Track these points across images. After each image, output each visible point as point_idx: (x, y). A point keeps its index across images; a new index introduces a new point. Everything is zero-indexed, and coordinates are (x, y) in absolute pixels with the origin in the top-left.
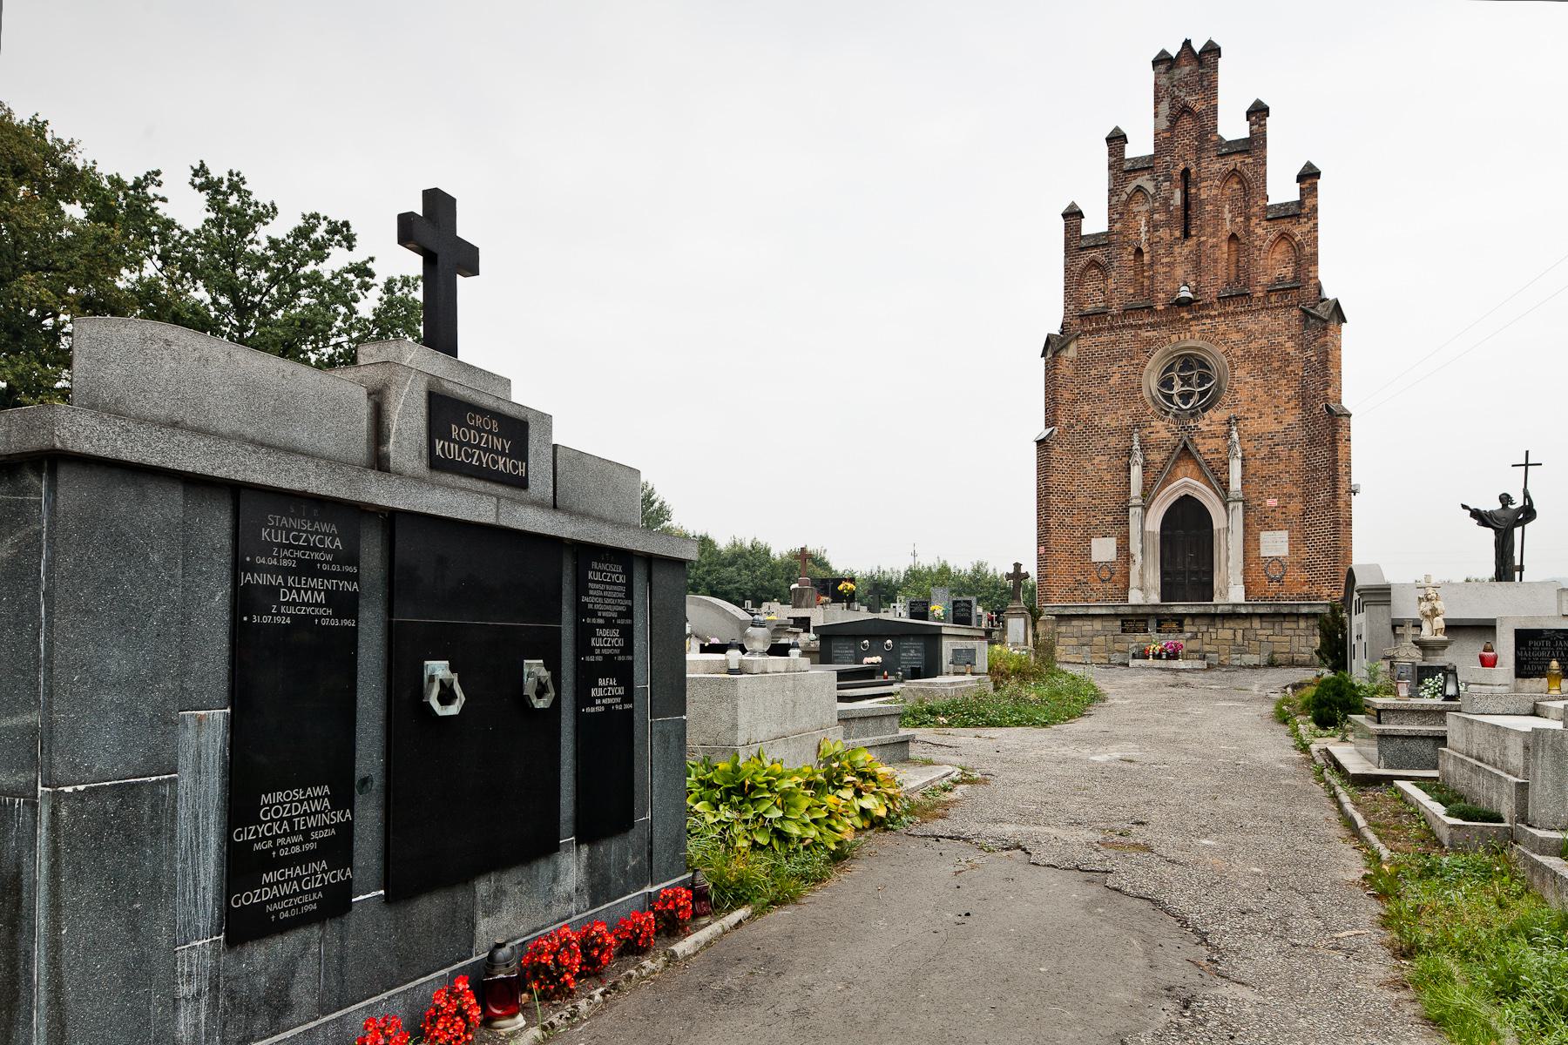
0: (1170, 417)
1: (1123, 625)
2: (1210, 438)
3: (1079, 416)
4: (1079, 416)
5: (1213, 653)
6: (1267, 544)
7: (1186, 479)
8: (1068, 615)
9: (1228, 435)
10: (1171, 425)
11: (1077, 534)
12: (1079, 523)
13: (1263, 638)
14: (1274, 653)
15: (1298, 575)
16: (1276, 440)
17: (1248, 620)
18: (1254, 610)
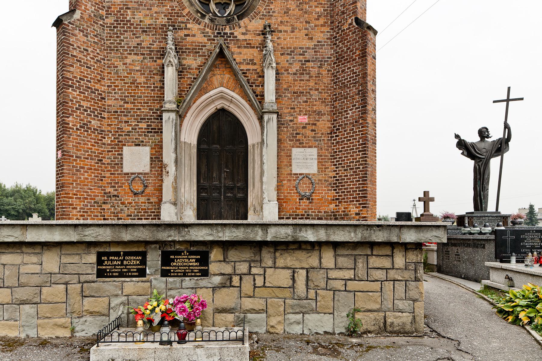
0: (207, 20)
1: (100, 262)
2: (245, 47)
3: (109, 8)
4: (109, 8)
5: (258, 312)
6: (298, 161)
7: (222, 89)
9: (263, 45)
10: (207, 30)
11: (107, 141)
12: (109, 129)
13: (339, 285)
14: (356, 310)
15: (325, 193)
16: (308, 56)
17: (316, 253)
18: (328, 235)
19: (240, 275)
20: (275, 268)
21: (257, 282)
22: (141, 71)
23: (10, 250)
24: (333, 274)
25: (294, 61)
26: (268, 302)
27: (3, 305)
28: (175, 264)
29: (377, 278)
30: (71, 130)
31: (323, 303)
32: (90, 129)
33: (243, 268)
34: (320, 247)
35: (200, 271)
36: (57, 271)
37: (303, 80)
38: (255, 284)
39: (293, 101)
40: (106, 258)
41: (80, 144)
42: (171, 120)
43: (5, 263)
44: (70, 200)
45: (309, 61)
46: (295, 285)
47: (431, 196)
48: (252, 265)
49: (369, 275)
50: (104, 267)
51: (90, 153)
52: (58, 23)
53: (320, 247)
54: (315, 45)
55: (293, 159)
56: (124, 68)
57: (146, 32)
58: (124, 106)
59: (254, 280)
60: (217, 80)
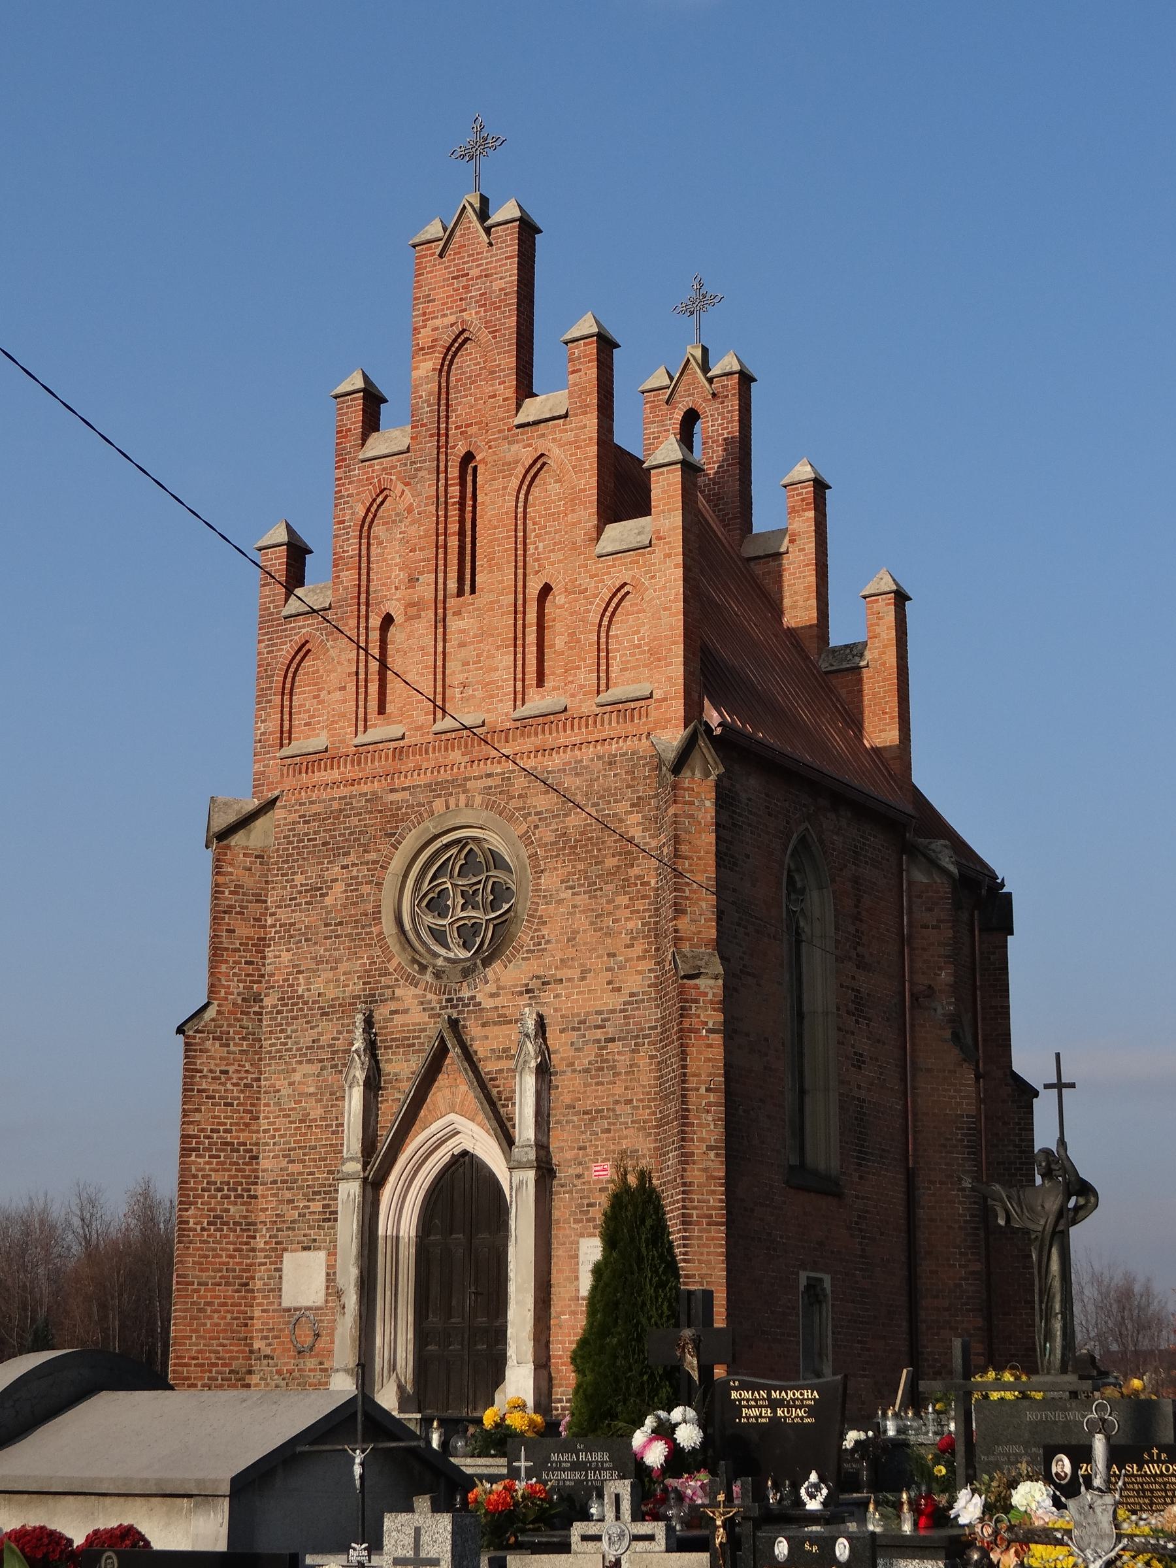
2: (495, 1023)
7: (452, 1117)
16: (610, 1031)
22: (317, 1094)
25: (585, 1043)
30: (191, 1234)
32: (227, 1224)
37: (602, 1084)
39: (582, 1132)
41: (207, 1257)
42: (352, 1197)
44: (185, 1369)
45: (613, 1040)
51: (225, 1273)
52: (180, 1030)
54: (625, 1003)
55: (580, 1262)
56: (290, 1091)
57: (327, 1014)
58: (286, 1169)
60: (444, 1099)
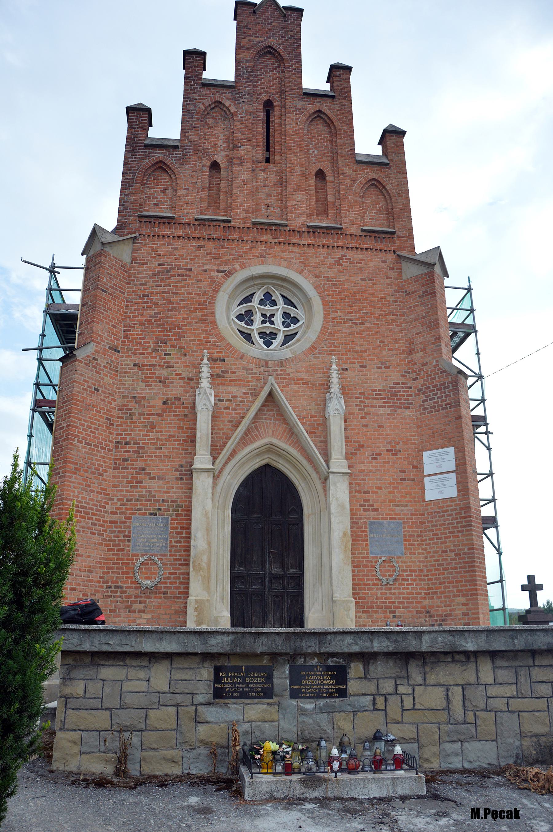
1: (217, 679)
8: (93, 654)
13: (499, 704)
17: (472, 666)
19: (384, 695)
20: (425, 685)
21: (405, 703)
23: (111, 662)
24: (493, 691)
26: (419, 728)
27: (100, 731)
28: (306, 682)
29: (542, 694)
31: (484, 727)
33: (388, 686)
34: (476, 658)
35: (338, 691)
36: (166, 689)
38: (403, 706)
40: (224, 674)
43: (105, 679)
46: (450, 706)
47: (537, 582)
48: (398, 683)
49: (533, 690)
50: (222, 686)
53: (476, 658)
59: (402, 701)
